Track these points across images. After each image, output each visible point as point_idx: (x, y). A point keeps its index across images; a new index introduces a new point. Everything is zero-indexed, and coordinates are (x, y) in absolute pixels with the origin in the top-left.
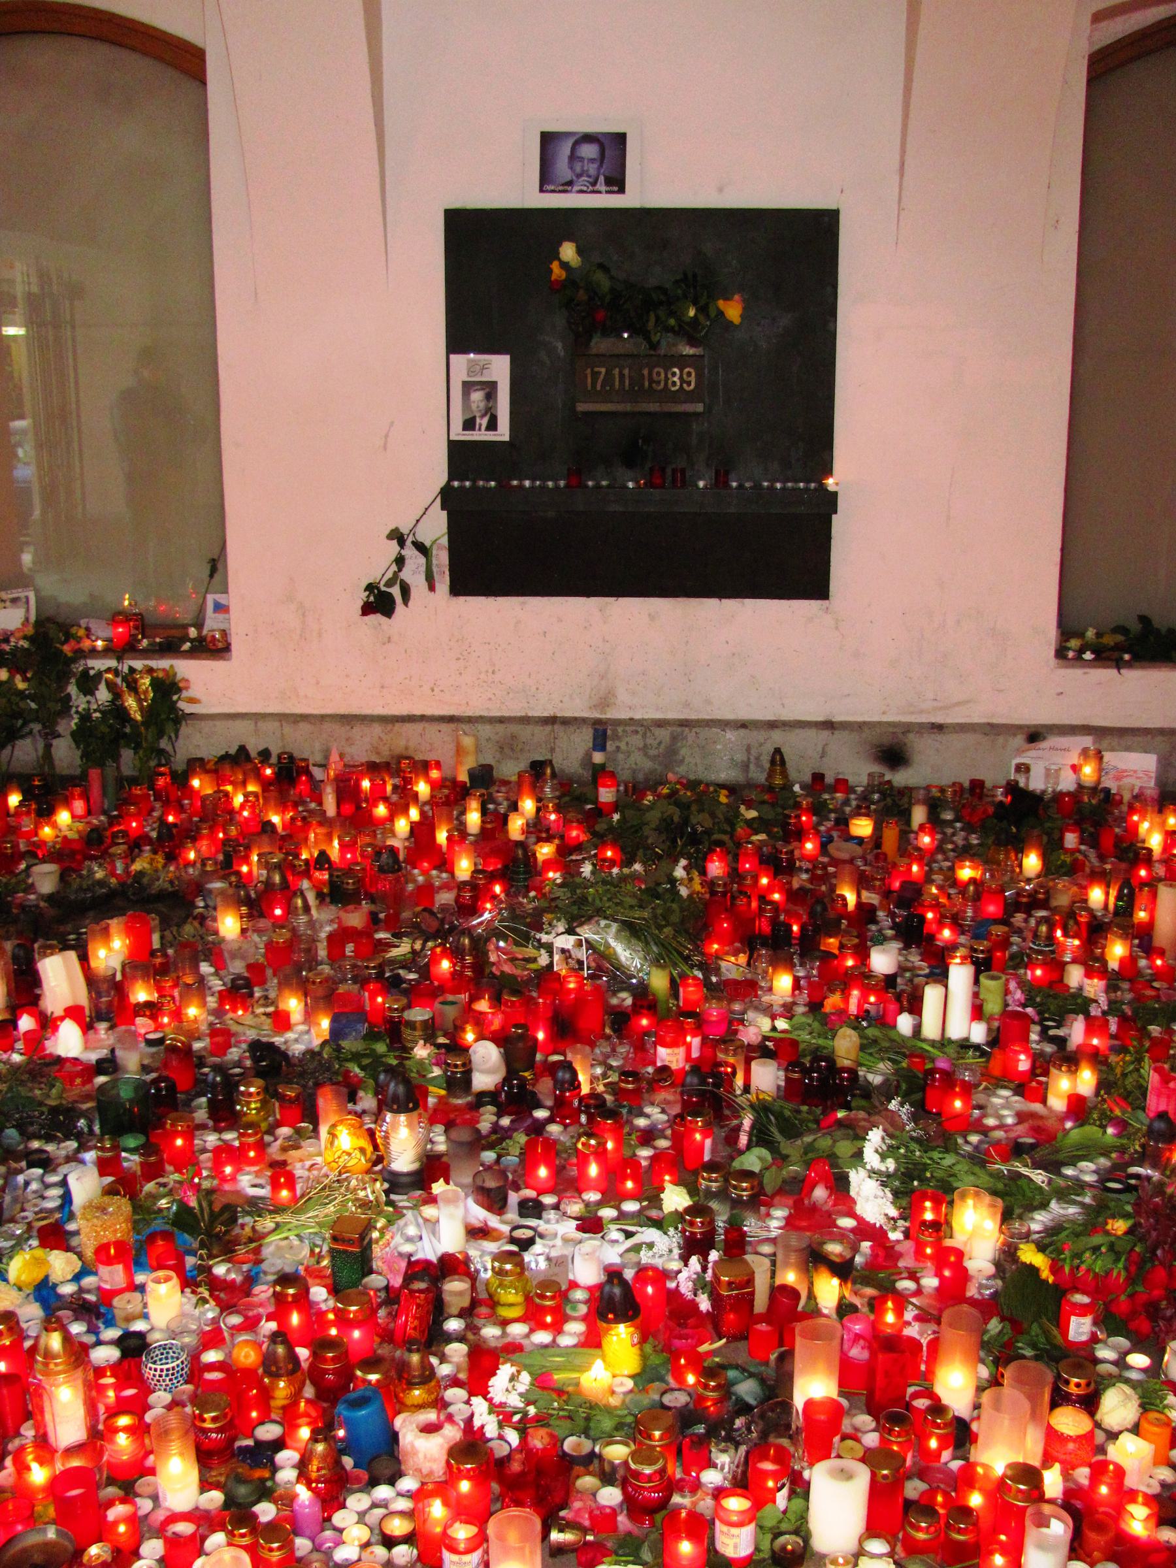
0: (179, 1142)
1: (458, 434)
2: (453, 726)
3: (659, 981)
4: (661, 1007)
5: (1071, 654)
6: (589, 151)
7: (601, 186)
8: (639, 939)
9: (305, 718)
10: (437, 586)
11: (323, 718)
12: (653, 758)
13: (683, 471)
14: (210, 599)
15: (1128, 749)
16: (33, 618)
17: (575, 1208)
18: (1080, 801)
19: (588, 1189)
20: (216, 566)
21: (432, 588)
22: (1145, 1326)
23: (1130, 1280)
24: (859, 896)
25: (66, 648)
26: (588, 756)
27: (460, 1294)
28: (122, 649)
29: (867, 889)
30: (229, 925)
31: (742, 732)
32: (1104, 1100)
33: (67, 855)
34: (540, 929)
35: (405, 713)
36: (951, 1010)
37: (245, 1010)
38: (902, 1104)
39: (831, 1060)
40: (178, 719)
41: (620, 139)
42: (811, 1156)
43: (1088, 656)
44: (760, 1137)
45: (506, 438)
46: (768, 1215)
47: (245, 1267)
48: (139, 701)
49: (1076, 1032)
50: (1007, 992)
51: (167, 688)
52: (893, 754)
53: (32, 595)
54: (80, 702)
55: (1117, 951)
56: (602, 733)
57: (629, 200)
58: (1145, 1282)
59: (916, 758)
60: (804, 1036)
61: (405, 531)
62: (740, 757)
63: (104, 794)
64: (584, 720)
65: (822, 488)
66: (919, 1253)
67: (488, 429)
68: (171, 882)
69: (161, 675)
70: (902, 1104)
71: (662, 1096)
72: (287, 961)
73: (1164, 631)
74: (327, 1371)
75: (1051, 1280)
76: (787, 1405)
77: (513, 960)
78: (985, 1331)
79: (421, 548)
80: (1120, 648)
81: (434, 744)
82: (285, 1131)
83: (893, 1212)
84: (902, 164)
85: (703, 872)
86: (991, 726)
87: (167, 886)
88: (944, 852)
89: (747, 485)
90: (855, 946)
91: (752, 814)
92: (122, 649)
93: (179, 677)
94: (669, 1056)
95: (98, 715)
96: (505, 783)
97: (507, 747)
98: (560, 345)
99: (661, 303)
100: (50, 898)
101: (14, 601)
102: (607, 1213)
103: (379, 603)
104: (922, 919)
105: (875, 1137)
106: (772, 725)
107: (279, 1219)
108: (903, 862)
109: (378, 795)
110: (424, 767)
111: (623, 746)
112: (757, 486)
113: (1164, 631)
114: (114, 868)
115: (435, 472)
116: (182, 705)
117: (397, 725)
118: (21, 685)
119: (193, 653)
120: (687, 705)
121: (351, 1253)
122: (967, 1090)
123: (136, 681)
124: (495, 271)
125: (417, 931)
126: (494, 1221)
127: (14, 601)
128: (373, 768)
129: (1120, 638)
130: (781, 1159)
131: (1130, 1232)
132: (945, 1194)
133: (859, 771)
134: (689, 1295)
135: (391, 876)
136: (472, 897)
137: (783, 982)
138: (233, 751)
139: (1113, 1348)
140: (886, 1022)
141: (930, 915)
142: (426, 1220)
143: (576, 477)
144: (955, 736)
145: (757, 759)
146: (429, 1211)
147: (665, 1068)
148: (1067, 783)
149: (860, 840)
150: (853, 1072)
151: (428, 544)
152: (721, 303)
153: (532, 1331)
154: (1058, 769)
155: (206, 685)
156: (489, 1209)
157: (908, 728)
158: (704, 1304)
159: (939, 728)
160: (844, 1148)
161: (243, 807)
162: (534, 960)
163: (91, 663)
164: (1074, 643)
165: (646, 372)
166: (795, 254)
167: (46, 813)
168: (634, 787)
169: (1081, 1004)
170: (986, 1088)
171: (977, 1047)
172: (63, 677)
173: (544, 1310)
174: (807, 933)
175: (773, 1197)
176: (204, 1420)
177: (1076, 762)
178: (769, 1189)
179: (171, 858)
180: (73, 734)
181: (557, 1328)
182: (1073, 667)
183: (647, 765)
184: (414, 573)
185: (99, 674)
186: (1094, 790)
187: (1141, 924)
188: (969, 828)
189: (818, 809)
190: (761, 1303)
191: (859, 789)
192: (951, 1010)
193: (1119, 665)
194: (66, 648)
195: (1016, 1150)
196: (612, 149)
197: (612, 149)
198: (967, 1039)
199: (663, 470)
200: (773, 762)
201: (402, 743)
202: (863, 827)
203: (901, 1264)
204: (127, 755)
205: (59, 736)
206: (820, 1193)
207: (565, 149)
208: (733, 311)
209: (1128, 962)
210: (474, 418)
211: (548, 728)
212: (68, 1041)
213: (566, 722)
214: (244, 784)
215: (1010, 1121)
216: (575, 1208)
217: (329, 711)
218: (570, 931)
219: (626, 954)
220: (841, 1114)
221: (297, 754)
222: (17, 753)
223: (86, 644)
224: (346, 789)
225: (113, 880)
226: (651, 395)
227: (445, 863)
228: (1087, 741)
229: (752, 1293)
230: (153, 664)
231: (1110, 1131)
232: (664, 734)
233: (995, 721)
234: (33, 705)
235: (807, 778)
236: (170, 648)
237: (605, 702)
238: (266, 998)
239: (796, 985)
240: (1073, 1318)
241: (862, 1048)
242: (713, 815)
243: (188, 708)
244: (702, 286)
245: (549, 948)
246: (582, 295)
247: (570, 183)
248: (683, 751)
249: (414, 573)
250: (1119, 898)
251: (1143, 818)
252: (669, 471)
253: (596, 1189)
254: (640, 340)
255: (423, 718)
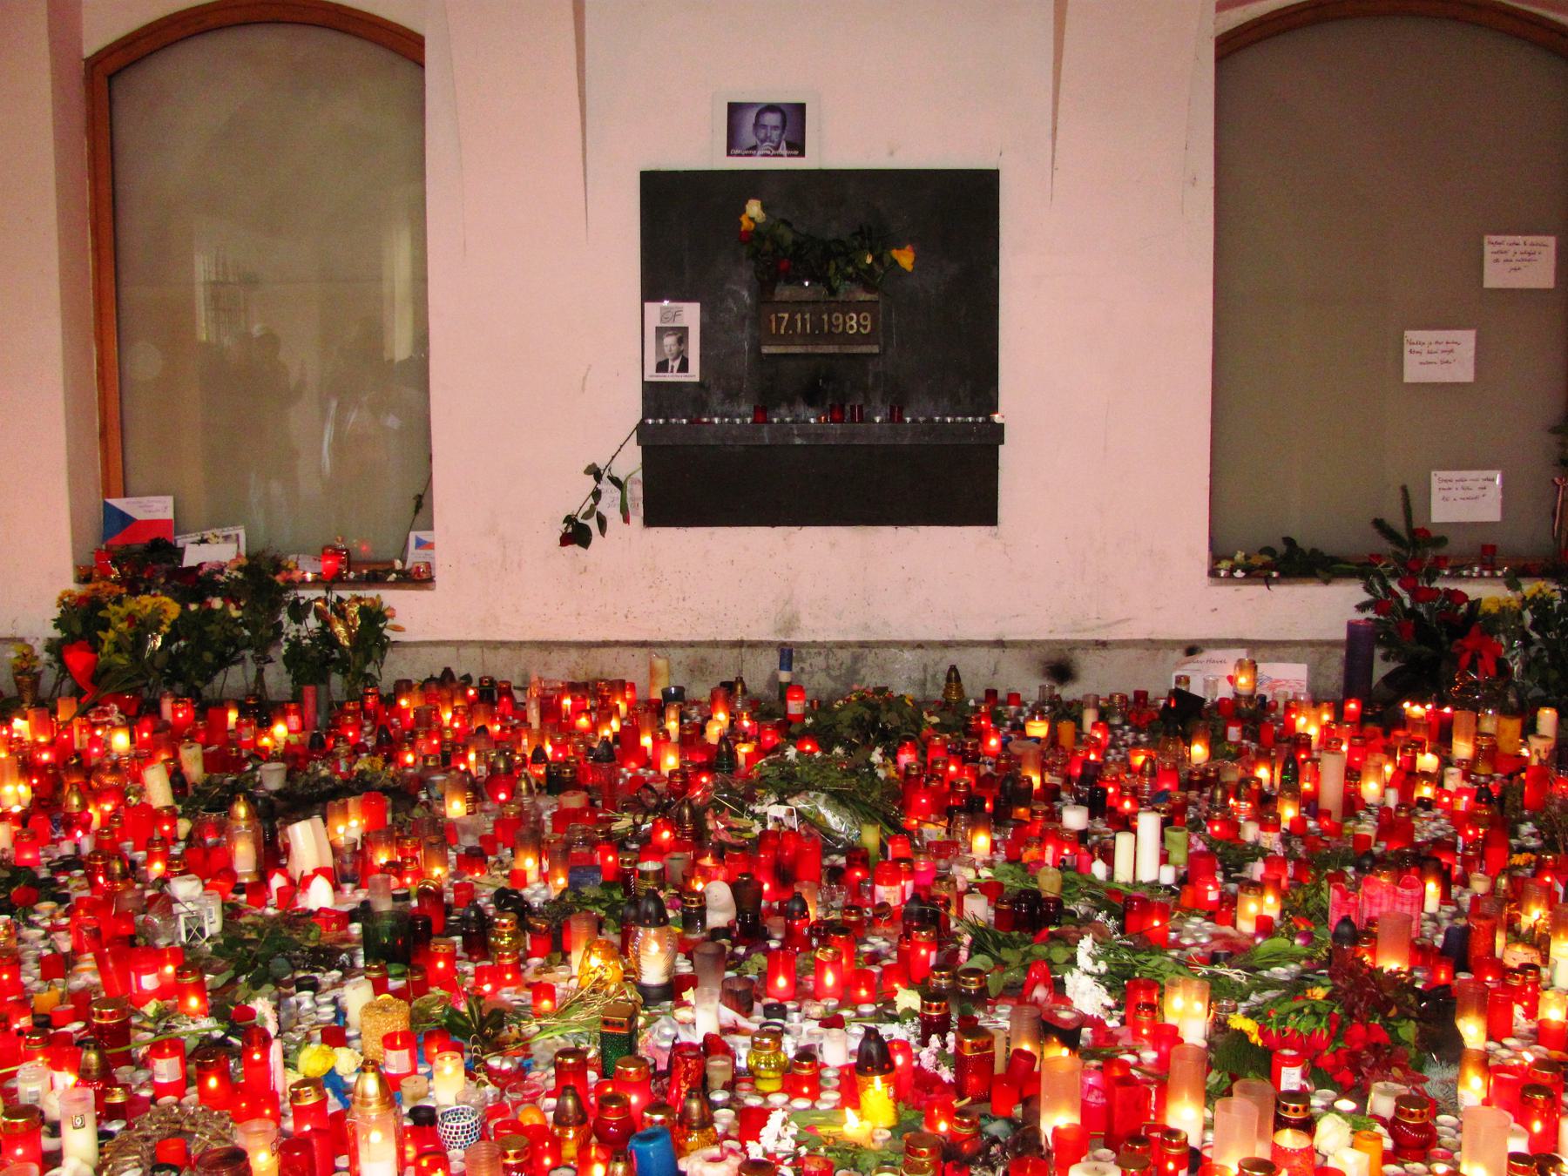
0: (441, 965)
1: (652, 375)
2: (645, 650)
3: (871, 837)
4: (872, 861)
5: (1222, 573)
6: (772, 119)
7: (783, 150)
8: (846, 806)
9: (504, 644)
10: (632, 518)
11: (522, 644)
12: (835, 679)
13: (861, 408)
14: (413, 535)
15: (1280, 660)
16: (243, 551)
17: (816, 1010)
18: (1239, 708)
19: (826, 996)
20: (421, 504)
21: (626, 520)
22: (1345, 1074)
23: (1333, 1037)
24: (1043, 780)
25: (279, 578)
26: (774, 676)
27: (723, 1068)
28: (329, 580)
29: (1050, 771)
30: (456, 808)
31: (919, 651)
32: (1289, 920)
33: (292, 757)
34: (753, 800)
35: (600, 639)
36: (1142, 855)
37: (482, 872)
38: (1108, 917)
39: (1036, 894)
40: (384, 645)
41: (800, 109)
42: (1029, 960)
43: (1239, 574)
44: (977, 948)
45: (697, 379)
46: (994, 1011)
47: (518, 1059)
48: (348, 628)
49: (1257, 870)
50: (1190, 845)
51: (374, 617)
52: (1060, 670)
53: (242, 533)
54: (290, 629)
55: (1288, 812)
56: (787, 654)
57: (813, 160)
58: (1345, 1038)
59: (1083, 674)
60: (1008, 881)
61: (601, 466)
62: (917, 675)
63: (317, 711)
64: (770, 644)
65: (989, 421)
66: (1136, 1034)
67: (679, 370)
68: (393, 780)
69: (368, 604)
70: (1108, 917)
71: (882, 929)
72: (516, 832)
73: (1307, 550)
74: (610, 1123)
75: (1260, 1043)
76: (1036, 1132)
77: (729, 829)
78: (1206, 1083)
79: (616, 481)
80: (1267, 567)
81: (631, 668)
82: (536, 961)
83: (1110, 1002)
84: (1055, 129)
85: (895, 762)
86: (1152, 641)
87: (389, 783)
88: (1115, 747)
89: (921, 419)
90: (1045, 813)
91: (935, 720)
92: (329, 580)
93: (385, 606)
94: (887, 894)
95: (308, 641)
96: (696, 703)
97: (698, 669)
98: (745, 294)
99: (840, 254)
100: (278, 793)
101: (227, 538)
102: (846, 1013)
103: (576, 534)
104: (1105, 791)
105: (1086, 945)
106: (946, 645)
107: (544, 1022)
108: (1080, 748)
109: (578, 711)
110: (621, 686)
111: (806, 666)
112: (930, 420)
113: (1307, 550)
114: (338, 767)
115: (631, 410)
116: (386, 632)
117: (594, 651)
118: (235, 613)
119: (397, 584)
120: (867, 627)
121: (620, 1038)
122: (1164, 912)
123: (344, 610)
124: (684, 225)
125: (637, 806)
126: (743, 1022)
127: (227, 538)
128: (572, 688)
129: (1267, 558)
130: (1002, 965)
131: (1328, 997)
132: (1155, 987)
133: (1031, 687)
134: (932, 1070)
135: (605, 766)
136: (684, 781)
137: (981, 842)
138: (438, 674)
139: (1322, 1097)
140: (1082, 869)
141: (1111, 790)
142: (682, 1023)
143: (761, 415)
144: (1118, 651)
145: (934, 676)
146: (682, 1014)
147: (884, 905)
148: (1225, 691)
149: (1038, 740)
150: (1058, 903)
151: (622, 479)
152: (895, 253)
153: (790, 1100)
154: (1216, 679)
155: (412, 615)
156: (738, 1011)
157: (1074, 645)
158: (947, 1075)
159: (1103, 644)
160: (1059, 954)
161: (452, 721)
162: (748, 830)
163: (301, 593)
164: (1225, 564)
165: (825, 317)
166: (959, 211)
167: (265, 725)
168: (819, 702)
169: (1257, 852)
170: (1180, 917)
171: (1167, 887)
172: (274, 607)
173: (800, 1081)
174: (1000, 801)
175: (996, 998)
176: (506, 1156)
177: (1231, 673)
178: (993, 993)
179: (389, 760)
180: (285, 658)
181: (814, 1095)
182: (1226, 584)
183: (830, 684)
184: (609, 505)
185: (309, 603)
186: (1250, 698)
187: (1306, 793)
188: (1137, 729)
189: (996, 718)
190: (999, 1067)
191: (1030, 704)
192: (1142, 855)
193: (1268, 581)
194: (279, 578)
195: (1213, 959)
196: (791, 122)
197: (791, 122)
198: (1157, 881)
199: (843, 406)
200: (949, 679)
201: (598, 669)
202: (1038, 729)
203: (1120, 1044)
204: (336, 680)
205: (271, 661)
206: (1040, 993)
207: (751, 117)
208: (906, 259)
209: (1298, 823)
210: (666, 361)
211: (736, 651)
212: (319, 895)
213: (753, 645)
214: (452, 700)
215: (1204, 940)
216: (816, 1010)
217: (527, 637)
218: (782, 802)
219: (834, 820)
220: (1052, 929)
221: (498, 678)
222: (230, 681)
223: (296, 576)
224: (549, 709)
225: (338, 777)
226: (830, 337)
227: (653, 763)
228: (1242, 653)
229: (993, 1055)
230: (359, 593)
231: (1298, 941)
232: (845, 655)
233: (1153, 637)
234: (247, 633)
235: (982, 695)
236: (376, 578)
237: (790, 624)
238: (501, 861)
239: (994, 847)
240: (1284, 1069)
241: (1063, 888)
242: (901, 716)
243: (394, 636)
244: (878, 238)
245: (763, 818)
246: (768, 246)
247: (755, 148)
248: (863, 672)
249: (609, 505)
250: (1284, 772)
251: (1298, 716)
252: (848, 408)
253: (832, 996)
254: (820, 287)
255: (617, 643)
